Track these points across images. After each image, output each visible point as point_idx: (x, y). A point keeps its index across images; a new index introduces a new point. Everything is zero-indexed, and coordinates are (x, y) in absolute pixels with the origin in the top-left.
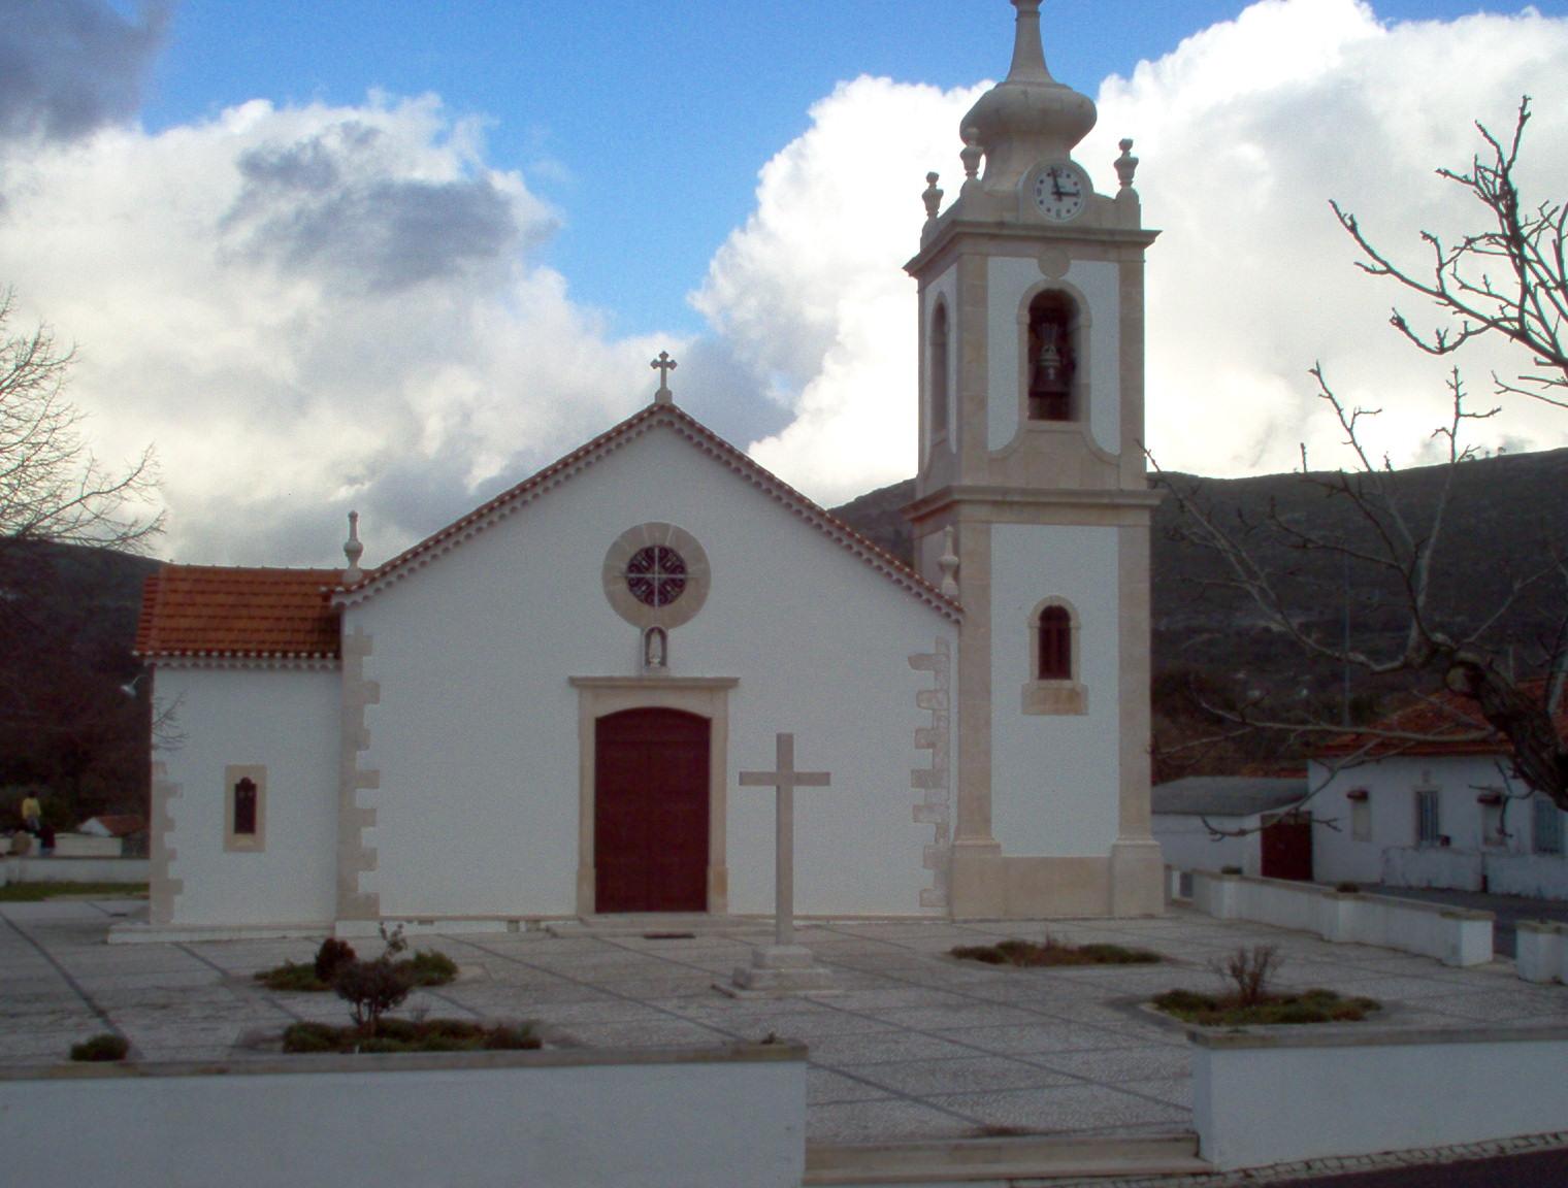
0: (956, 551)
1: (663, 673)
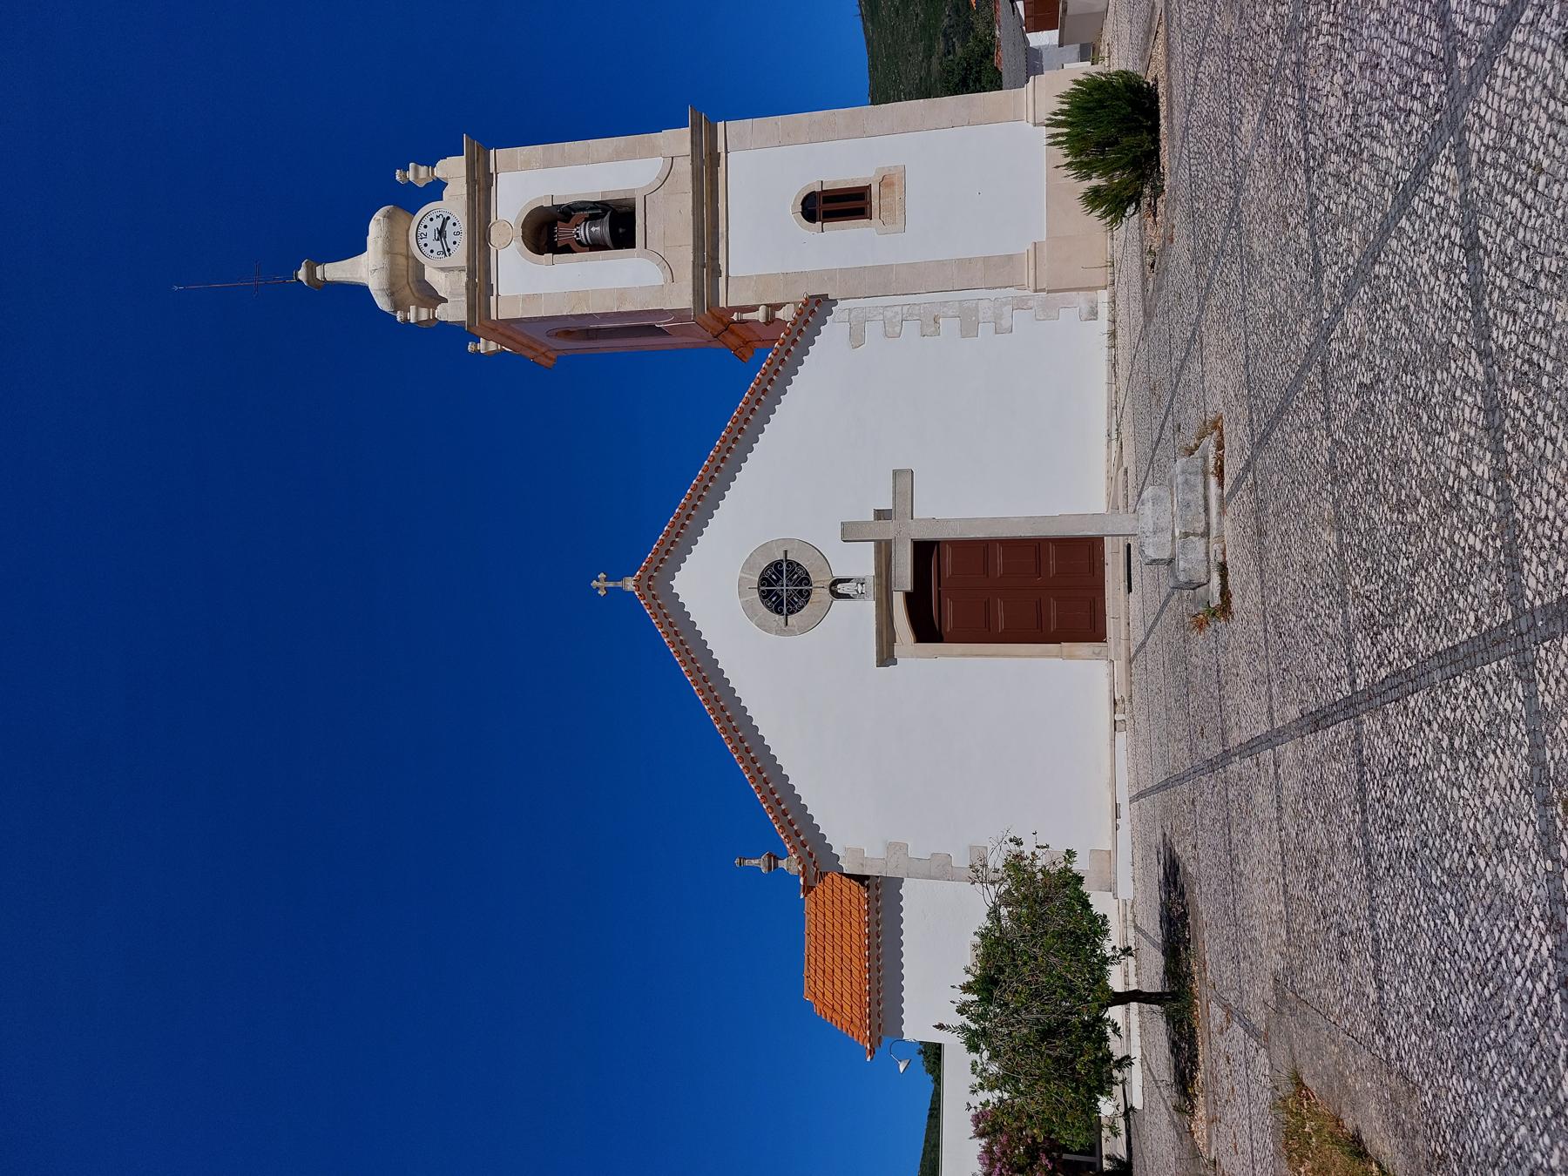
0: (755, 309)
1: (870, 582)
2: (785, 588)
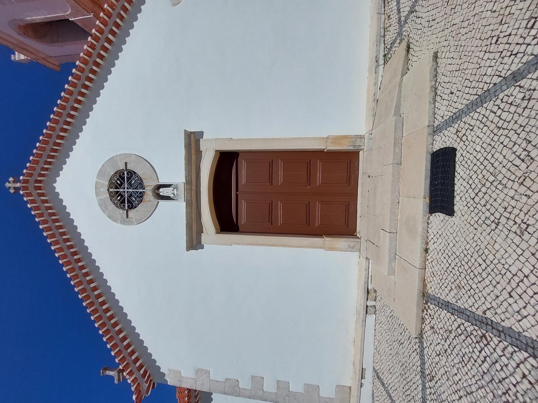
1: (182, 188)
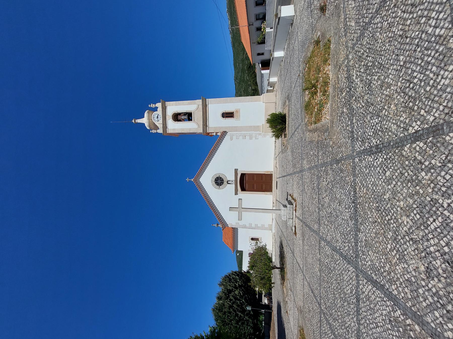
0: (214, 133)
2: (219, 181)
